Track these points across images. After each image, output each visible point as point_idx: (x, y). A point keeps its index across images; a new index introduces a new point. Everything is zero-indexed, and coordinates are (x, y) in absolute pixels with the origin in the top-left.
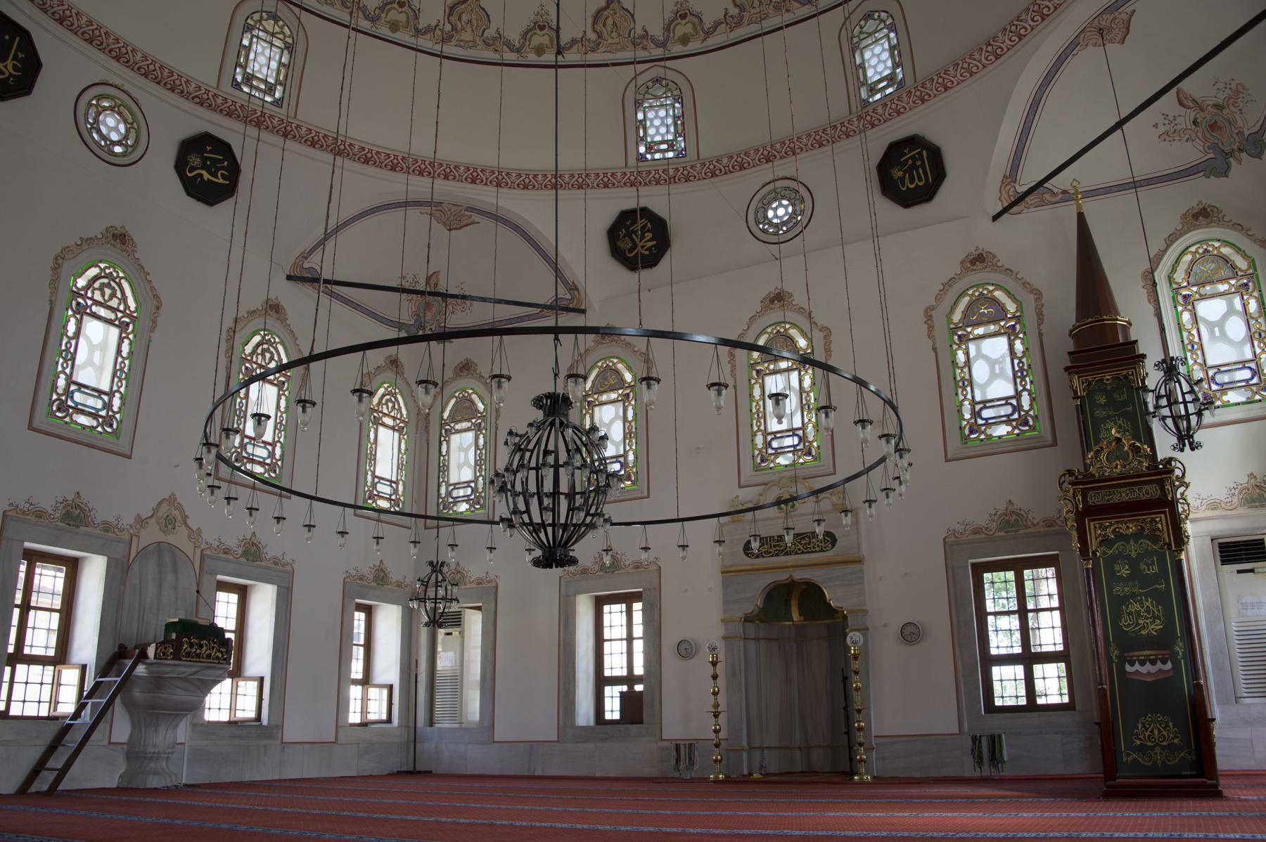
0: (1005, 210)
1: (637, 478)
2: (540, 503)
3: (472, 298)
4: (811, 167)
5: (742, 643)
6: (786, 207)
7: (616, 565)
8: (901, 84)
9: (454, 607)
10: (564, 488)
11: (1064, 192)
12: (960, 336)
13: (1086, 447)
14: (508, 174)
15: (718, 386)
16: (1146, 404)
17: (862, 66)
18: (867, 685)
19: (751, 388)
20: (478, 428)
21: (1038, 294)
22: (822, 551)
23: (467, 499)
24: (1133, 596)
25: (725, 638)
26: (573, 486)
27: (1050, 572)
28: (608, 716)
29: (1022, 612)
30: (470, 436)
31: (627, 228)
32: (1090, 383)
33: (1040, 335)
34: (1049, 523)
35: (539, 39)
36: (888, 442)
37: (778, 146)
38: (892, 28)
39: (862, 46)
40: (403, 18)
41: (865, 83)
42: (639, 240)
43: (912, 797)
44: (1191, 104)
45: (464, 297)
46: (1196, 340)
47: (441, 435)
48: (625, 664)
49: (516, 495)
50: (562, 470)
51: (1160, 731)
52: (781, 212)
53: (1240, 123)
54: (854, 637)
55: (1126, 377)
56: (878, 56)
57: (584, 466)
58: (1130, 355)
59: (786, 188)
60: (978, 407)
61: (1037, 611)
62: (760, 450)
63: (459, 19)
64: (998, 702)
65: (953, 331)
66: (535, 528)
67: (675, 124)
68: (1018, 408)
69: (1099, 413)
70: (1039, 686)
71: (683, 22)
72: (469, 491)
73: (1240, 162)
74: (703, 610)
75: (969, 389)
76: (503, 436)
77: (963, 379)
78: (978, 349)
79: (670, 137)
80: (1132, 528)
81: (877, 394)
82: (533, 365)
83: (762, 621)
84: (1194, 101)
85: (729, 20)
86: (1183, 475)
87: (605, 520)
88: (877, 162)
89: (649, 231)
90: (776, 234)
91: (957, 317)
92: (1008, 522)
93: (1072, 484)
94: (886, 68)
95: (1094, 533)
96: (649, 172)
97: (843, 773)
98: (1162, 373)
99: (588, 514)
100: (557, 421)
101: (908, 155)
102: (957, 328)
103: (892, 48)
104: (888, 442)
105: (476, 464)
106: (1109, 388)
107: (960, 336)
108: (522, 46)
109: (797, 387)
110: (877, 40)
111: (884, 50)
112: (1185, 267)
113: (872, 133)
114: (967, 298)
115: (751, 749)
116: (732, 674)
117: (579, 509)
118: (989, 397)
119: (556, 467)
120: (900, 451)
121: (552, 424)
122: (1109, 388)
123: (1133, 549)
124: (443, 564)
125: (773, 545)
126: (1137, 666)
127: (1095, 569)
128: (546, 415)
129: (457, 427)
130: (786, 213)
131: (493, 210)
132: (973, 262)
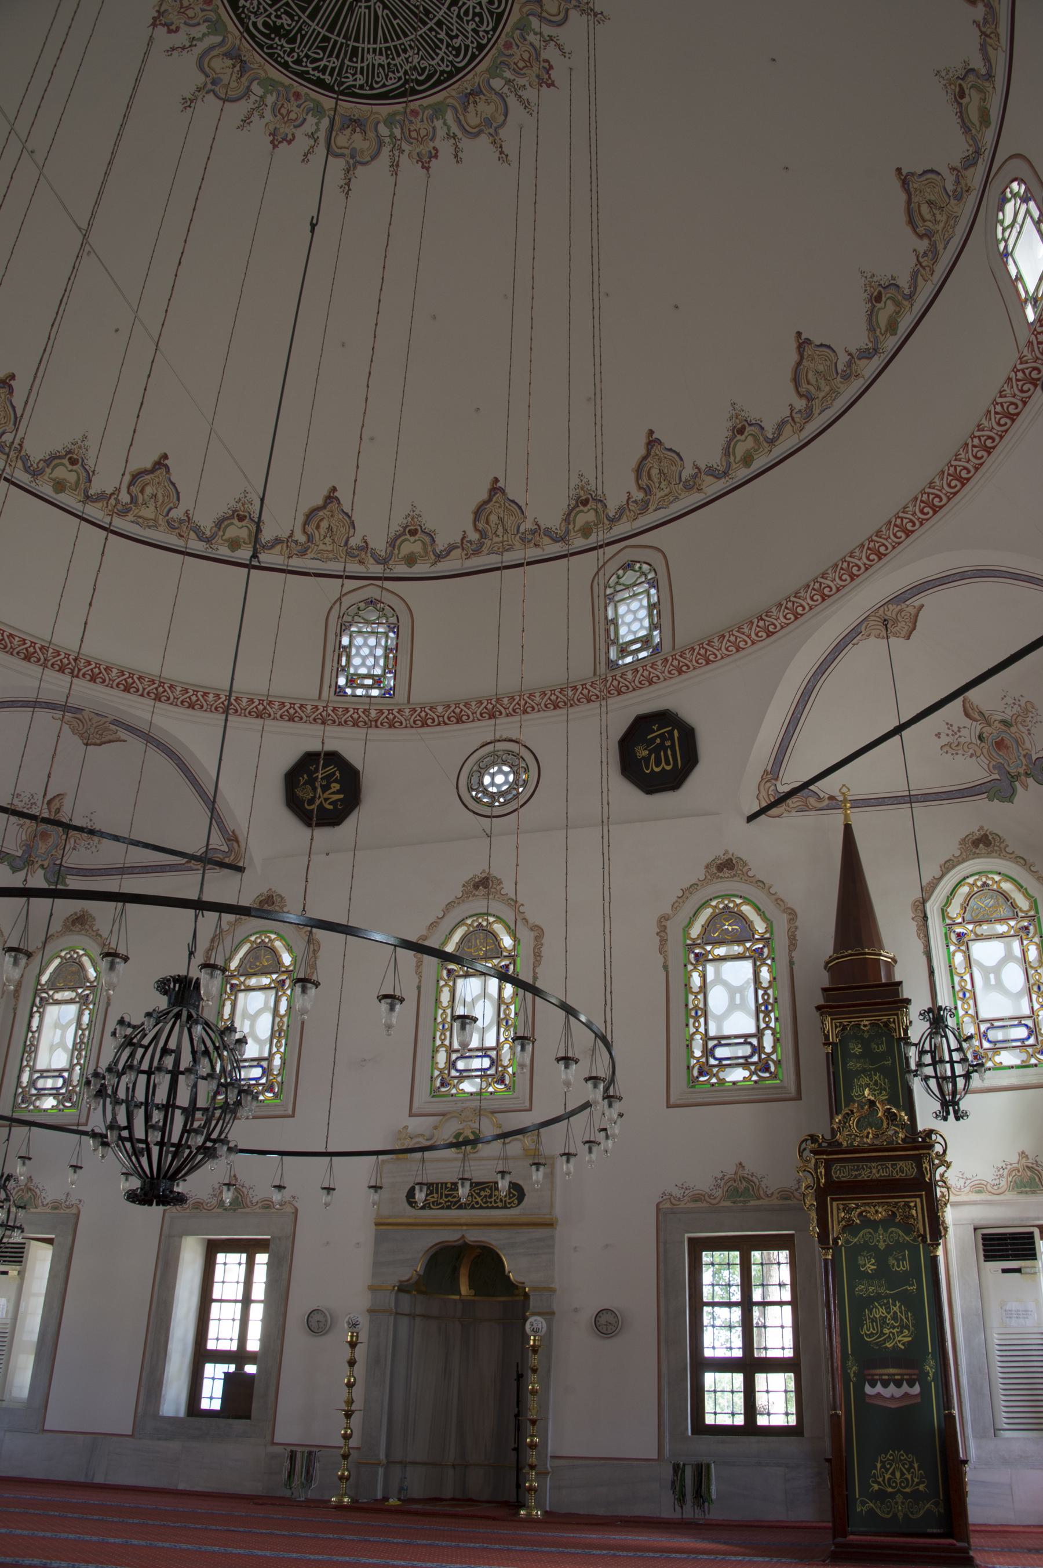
0: (763, 811)
1: (281, 1090)
2: (148, 1117)
3: (102, 835)
4: (539, 730)
5: (392, 1318)
6: (506, 774)
7: (239, 1202)
8: (657, 650)
9: (16, 1237)
10: (183, 1099)
11: (832, 798)
12: (696, 955)
13: (835, 1108)
14: (171, 687)
15: (392, 999)
16: (907, 1059)
17: (614, 622)
18: (546, 1387)
19: (439, 991)
20: (83, 1001)
21: (793, 915)
22: (505, 1207)
23: (55, 1093)
24: (878, 1297)
25: (370, 1311)
26: (194, 1100)
27: (783, 1255)
28: (205, 1405)
29: (747, 1304)
30: (72, 1010)
31: (310, 774)
32: (844, 1028)
33: (791, 963)
34: (786, 1195)
35: (238, 530)
36: (595, 1086)
37: (506, 701)
38: (654, 584)
39: (617, 598)
40: (72, 478)
41: (615, 642)
42: (322, 791)
43: (591, 1546)
44: (977, 716)
45: (92, 832)
46: (969, 987)
47: (34, 1004)
48: (236, 1336)
49: (117, 1102)
50: (181, 1078)
51: (902, 1474)
52: (500, 779)
53: (1028, 745)
54: (535, 1323)
55: (886, 1024)
56: (635, 612)
57: (211, 1076)
58: (891, 998)
59: (509, 752)
60: (711, 1044)
61: (764, 1304)
62: (441, 1071)
63: (142, 491)
64: (709, 1420)
65: (690, 948)
66: (138, 1149)
67: (386, 657)
68: (758, 1049)
69: (852, 1065)
70: (761, 1400)
71: (412, 539)
72: (60, 1082)
73: (1026, 787)
74: (348, 1262)
75: (702, 1020)
76: (112, 1024)
77: (696, 1008)
78: (717, 973)
79: (378, 671)
80: (882, 1213)
81: (588, 1025)
82: (160, 943)
83: (420, 1292)
84: (981, 713)
85: (466, 545)
86: (945, 1151)
87: (230, 1149)
88: (619, 737)
89: (336, 781)
90: (490, 805)
91: (695, 931)
92: (736, 1189)
93: (815, 1152)
94: (642, 627)
95: (836, 1213)
96: (347, 710)
97: (506, 1504)
98: (928, 1024)
99: (208, 1139)
100: (185, 1013)
101: (656, 733)
102: (695, 945)
103: (651, 607)
104: (595, 1086)
105: (74, 1048)
106: (866, 1035)
107: (696, 955)
108: (214, 536)
109: (496, 995)
110: (635, 595)
111: (642, 607)
112: (961, 900)
113: (615, 702)
114: (709, 911)
115: (390, 1463)
116: (375, 1360)
117: (197, 1132)
118: (726, 1033)
119: (175, 1074)
120: (610, 1098)
121: (178, 1016)
122: (866, 1035)
123: (881, 1239)
124: (9, 1177)
125: (442, 1194)
126: (879, 1388)
127: (835, 1262)
128: (172, 1004)
129: (58, 996)
130: (506, 782)
131: (145, 727)
132: (720, 868)
